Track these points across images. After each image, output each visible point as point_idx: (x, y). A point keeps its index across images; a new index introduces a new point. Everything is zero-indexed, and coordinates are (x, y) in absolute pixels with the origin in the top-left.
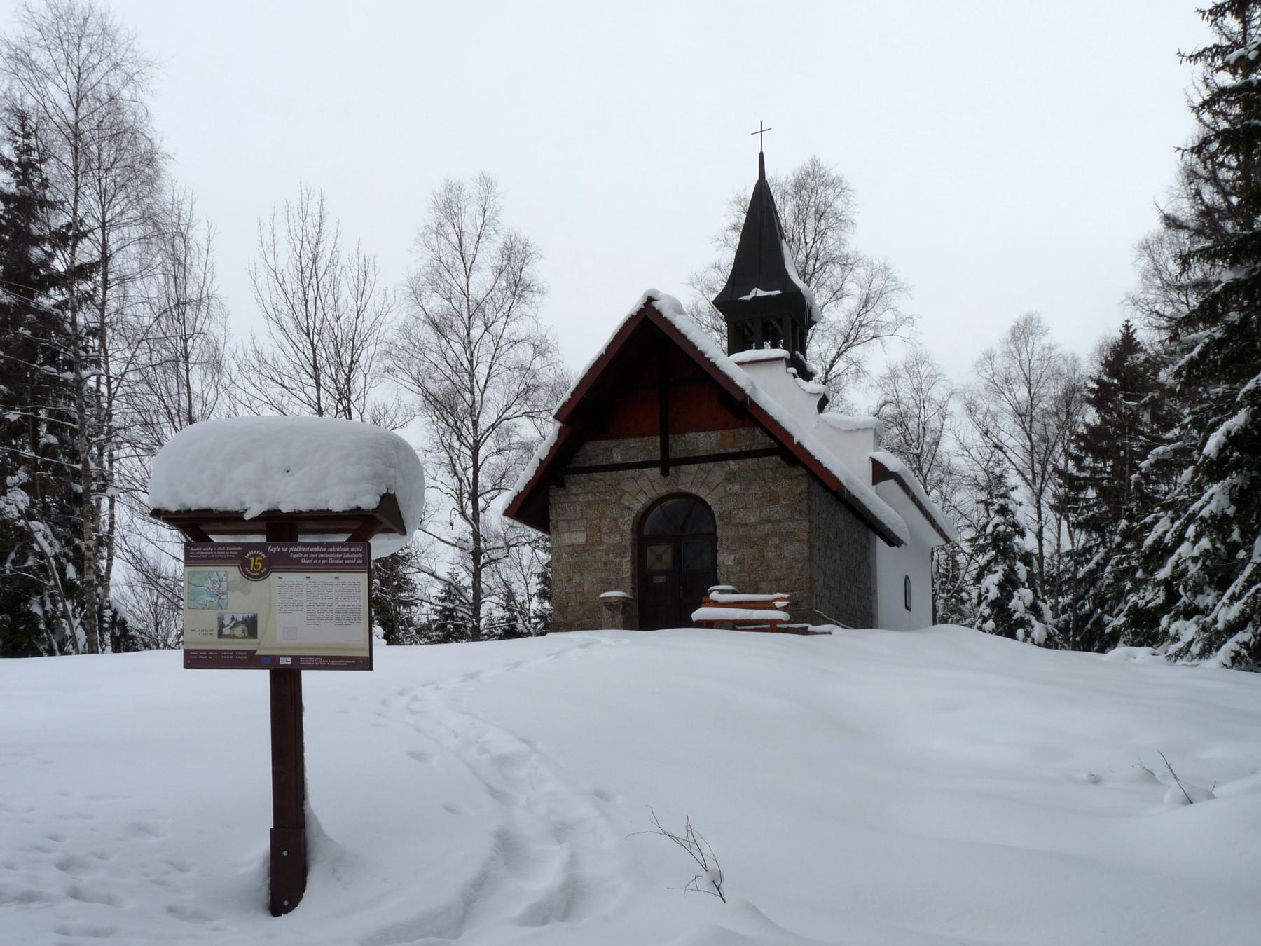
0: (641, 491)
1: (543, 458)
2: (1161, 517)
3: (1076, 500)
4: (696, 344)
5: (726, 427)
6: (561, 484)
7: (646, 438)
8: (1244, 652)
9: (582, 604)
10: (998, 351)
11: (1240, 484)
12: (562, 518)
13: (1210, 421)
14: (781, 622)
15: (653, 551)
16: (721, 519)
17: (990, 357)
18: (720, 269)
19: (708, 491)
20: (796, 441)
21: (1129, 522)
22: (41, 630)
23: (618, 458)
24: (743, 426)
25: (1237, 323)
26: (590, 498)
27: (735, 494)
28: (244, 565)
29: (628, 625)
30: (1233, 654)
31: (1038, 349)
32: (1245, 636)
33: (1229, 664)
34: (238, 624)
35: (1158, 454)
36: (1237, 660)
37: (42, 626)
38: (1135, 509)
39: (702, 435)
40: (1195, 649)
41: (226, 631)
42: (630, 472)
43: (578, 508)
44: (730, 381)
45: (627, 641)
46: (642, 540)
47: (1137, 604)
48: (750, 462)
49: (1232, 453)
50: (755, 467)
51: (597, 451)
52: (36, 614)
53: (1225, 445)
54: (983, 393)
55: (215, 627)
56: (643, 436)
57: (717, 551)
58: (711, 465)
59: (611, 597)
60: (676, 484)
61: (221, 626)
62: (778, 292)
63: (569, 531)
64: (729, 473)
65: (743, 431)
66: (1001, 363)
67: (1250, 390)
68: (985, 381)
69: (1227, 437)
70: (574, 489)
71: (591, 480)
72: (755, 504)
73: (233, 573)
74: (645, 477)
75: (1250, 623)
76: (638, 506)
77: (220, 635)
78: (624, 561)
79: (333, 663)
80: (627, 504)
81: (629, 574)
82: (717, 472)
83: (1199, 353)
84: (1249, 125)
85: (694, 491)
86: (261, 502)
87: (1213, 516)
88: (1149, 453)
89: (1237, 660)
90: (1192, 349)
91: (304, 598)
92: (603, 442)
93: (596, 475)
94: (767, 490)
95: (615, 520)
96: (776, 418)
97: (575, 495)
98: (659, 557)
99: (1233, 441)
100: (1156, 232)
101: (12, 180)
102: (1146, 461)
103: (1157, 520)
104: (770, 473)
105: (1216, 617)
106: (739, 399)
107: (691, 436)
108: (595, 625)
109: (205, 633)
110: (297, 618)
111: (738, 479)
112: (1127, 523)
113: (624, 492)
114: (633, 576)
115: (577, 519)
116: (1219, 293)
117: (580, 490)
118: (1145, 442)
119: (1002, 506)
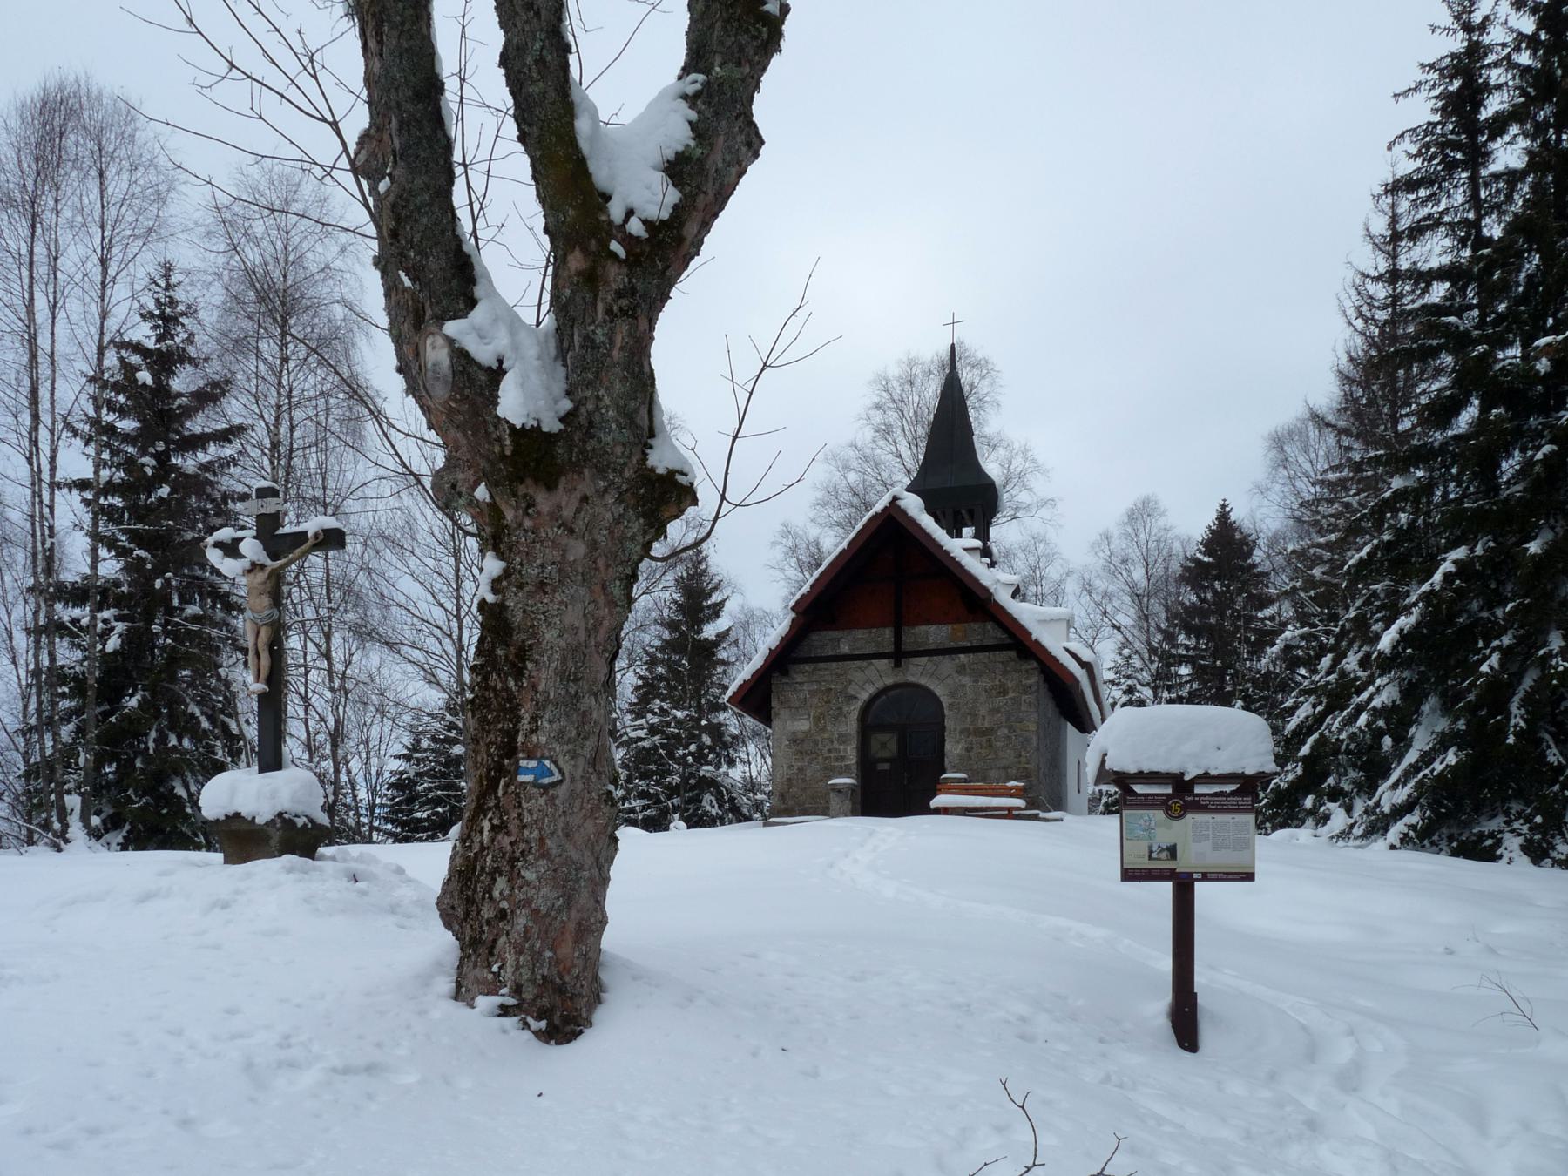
1: (773, 648)
2: (1303, 703)
3: (1168, 677)
4: (942, 543)
5: (957, 620)
6: (785, 673)
7: (874, 630)
8: (1412, 833)
9: (804, 790)
10: (1115, 532)
11: (1409, 677)
14: (1019, 809)
15: (877, 739)
16: (950, 710)
17: (1107, 537)
18: (856, 447)
20: (1034, 637)
22: (187, 814)
23: (845, 649)
24: (974, 620)
25: (1405, 527)
28: (1167, 810)
29: (855, 812)
30: (1402, 836)
31: (1154, 531)
32: (1414, 818)
33: (1398, 845)
34: (1163, 850)
35: (1286, 639)
36: (1405, 840)
37: (189, 810)
39: (933, 628)
40: (1357, 831)
41: (1154, 855)
42: (858, 663)
44: (975, 580)
45: (889, 829)
46: (869, 725)
47: (1279, 786)
48: (981, 655)
49: (1404, 649)
50: (986, 661)
51: (823, 641)
52: (181, 797)
53: (1398, 642)
54: (1101, 573)
56: (873, 627)
57: (945, 740)
58: (941, 658)
59: (840, 784)
61: (1151, 852)
65: (975, 626)
66: (1119, 544)
67: (1424, 592)
68: (1102, 561)
69: (1400, 634)
70: (799, 678)
73: (1159, 815)
74: (872, 667)
75: (1417, 807)
76: (864, 696)
77: (1150, 858)
78: (849, 749)
79: (1230, 877)
81: (854, 761)
82: (947, 664)
83: (1368, 553)
84: (1424, 344)
85: (923, 681)
86: (1197, 767)
87: (1384, 706)
89: (1405, 840)
90: (1361, 550)
91: (1210, 832)
92: (830, 632)
93: (822, 665)
96: (1015, 616)
97: (800, 683)
98: (883, 745)
99: (1405, 638)
100: (1286, 427)
101: (151, 333)
103: (1296, 706)
104: (1000, 666)
105: (1379, 801)
106: (983, 596)
107: (921, 629)
108: (824, 811)
109: (1139, 856)
110: (1206, 847)
111: (968, 671)
113: (851, 682)
114: (857, 763)
117: (805, 679)
119: (1129, 686)
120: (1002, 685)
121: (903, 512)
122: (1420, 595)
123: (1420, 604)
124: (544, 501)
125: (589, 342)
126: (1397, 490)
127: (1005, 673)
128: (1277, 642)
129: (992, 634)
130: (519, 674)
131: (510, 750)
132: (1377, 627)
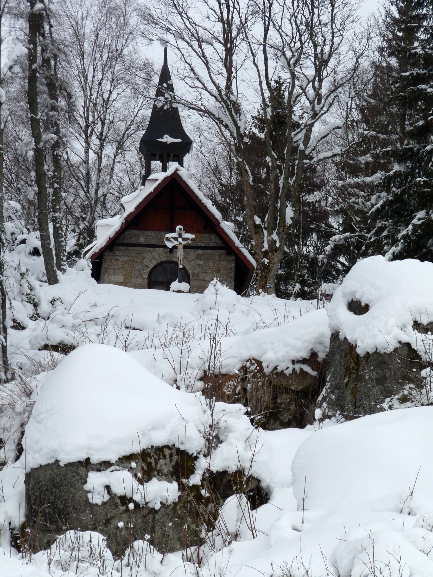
0: (153, 258)
1: (111, 237)
4: (198, 195)
7: (157, 232)
12: (110, 267)
13: (384, 243)
16: (193, 277)
19: (187, 262)
21: (301, 286)
23: (142, 240)
24: (206, 233)
26: (126, 258)
27: (200, 265)
38: (306, 276)
42: (148, 249)
43: (120, 263)
48: (209, 251)
55: (156, 318)
56: (156, 230)
60: (172, 257)
62: (179, 140)
63: (114, 274)
64: (197, 255)
65: (206, 235)
67: (404, 235)
70: (118, 253)
71: (127, 249)
72: (210, 271)
74: (156, 252)
76: (152, 266)
80: (146, 264)
83: (381, 205)
88: (329, 240)
92: (135, 231)
93: (130, 248)
94: (215, 265)
95: (139, 271)
97: (118, 256)
102: (329, 246)
112: (300, 287)
113: (144, 258)
115: (119, 269)
116: (392, 175)
117: (121, 254)
118: (325, 228)
120: (218, 266)
121: (180, 177)
122: (402, 236)
123: (402, 241)
124: (275, 254)
125: (282, 237)
126: (396, 171)
127: (220, 260)
128: (330, 242)
129: (214, 240)
130: (268, 273)
131: (266, 283)
132: (386, 248)
